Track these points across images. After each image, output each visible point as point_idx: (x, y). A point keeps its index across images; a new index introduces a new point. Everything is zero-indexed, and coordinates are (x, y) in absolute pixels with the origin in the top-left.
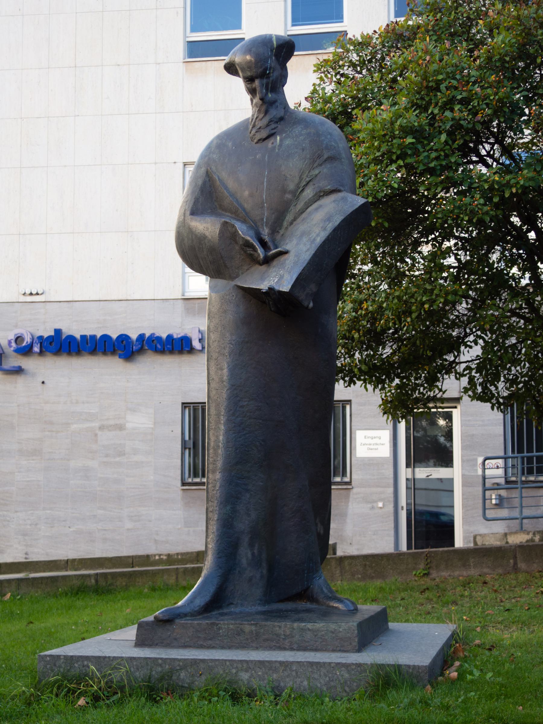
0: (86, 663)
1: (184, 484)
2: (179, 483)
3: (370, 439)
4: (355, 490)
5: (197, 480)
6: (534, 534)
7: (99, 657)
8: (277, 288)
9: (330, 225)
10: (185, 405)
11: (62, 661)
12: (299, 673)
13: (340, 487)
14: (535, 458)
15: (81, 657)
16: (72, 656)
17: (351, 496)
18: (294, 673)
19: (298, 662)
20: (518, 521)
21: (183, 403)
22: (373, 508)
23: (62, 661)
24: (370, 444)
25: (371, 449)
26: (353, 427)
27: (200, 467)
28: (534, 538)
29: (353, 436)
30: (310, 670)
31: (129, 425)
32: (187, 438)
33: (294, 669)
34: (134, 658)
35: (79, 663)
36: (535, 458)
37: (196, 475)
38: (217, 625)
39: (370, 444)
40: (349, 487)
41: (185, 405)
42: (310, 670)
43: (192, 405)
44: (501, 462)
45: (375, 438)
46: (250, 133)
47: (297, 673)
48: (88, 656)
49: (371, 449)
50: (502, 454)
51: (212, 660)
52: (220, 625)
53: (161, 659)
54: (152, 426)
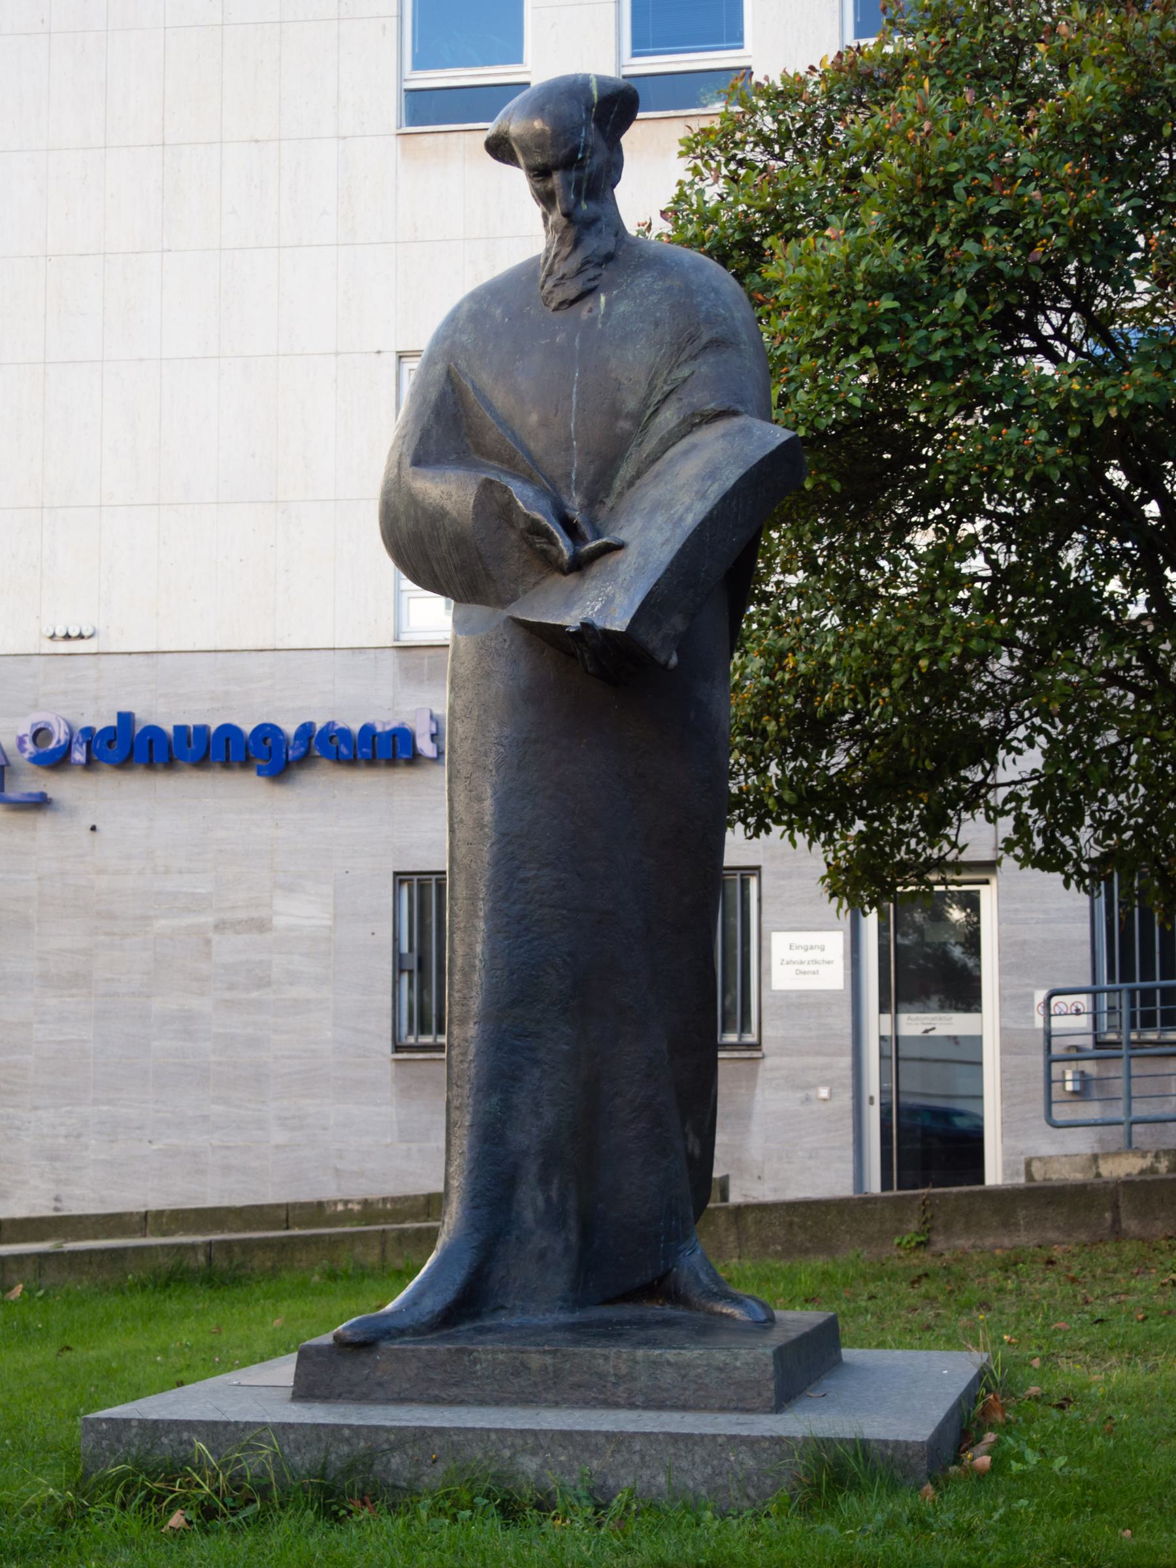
0: (185, 1436)
1: (398, 1048)
2: (388, 1046)
3: (801, 951)
4: (768, 1062)
5: (427, 1039)
6: (1157, 1156)
7: (215, 1424)
8: (599, 624)
9: (716, 486)
10: (400, 878)
11: (134, 1431)
12: (647, 1458)
13: (736, 1054)
14: (1158, 993)
15: (175, 1422)
16: (156, 1422)
17: (760, 1074)
18: (636, 1458)
19: (645, 1434)
20: (1121, 1128)
21: (396, 874)
22: (807, 1099)
23: (134, 1431)
24: (802, 963)
25: (804, 973)
26: (764, 926)
27: (434, 1011)
28: (1157, 1165)
29: (764, 943)
30: (672, 1451)
31: (279, 921)
32: (405, 948)
33: (638, 1448)
34: (289, 1424)
35: (171, 1436)
36: (1158, 993)
37: (424, 1029)
38: (470, 1354)
39: (802, 963)
40: (756, 1054)
41: (400, 878)
42: (672, 1451)
43: (415, 878)
44: (1084, 1001)
45: (812, 948)
46: (542, 287)
47: (643, 1457)
48: (190, 1421)
49: (804, 973)
50: (1087, 983)
51: (458, 1429)
52: (476, 1354)
53: (349, 1427)
54: (330, 923)
